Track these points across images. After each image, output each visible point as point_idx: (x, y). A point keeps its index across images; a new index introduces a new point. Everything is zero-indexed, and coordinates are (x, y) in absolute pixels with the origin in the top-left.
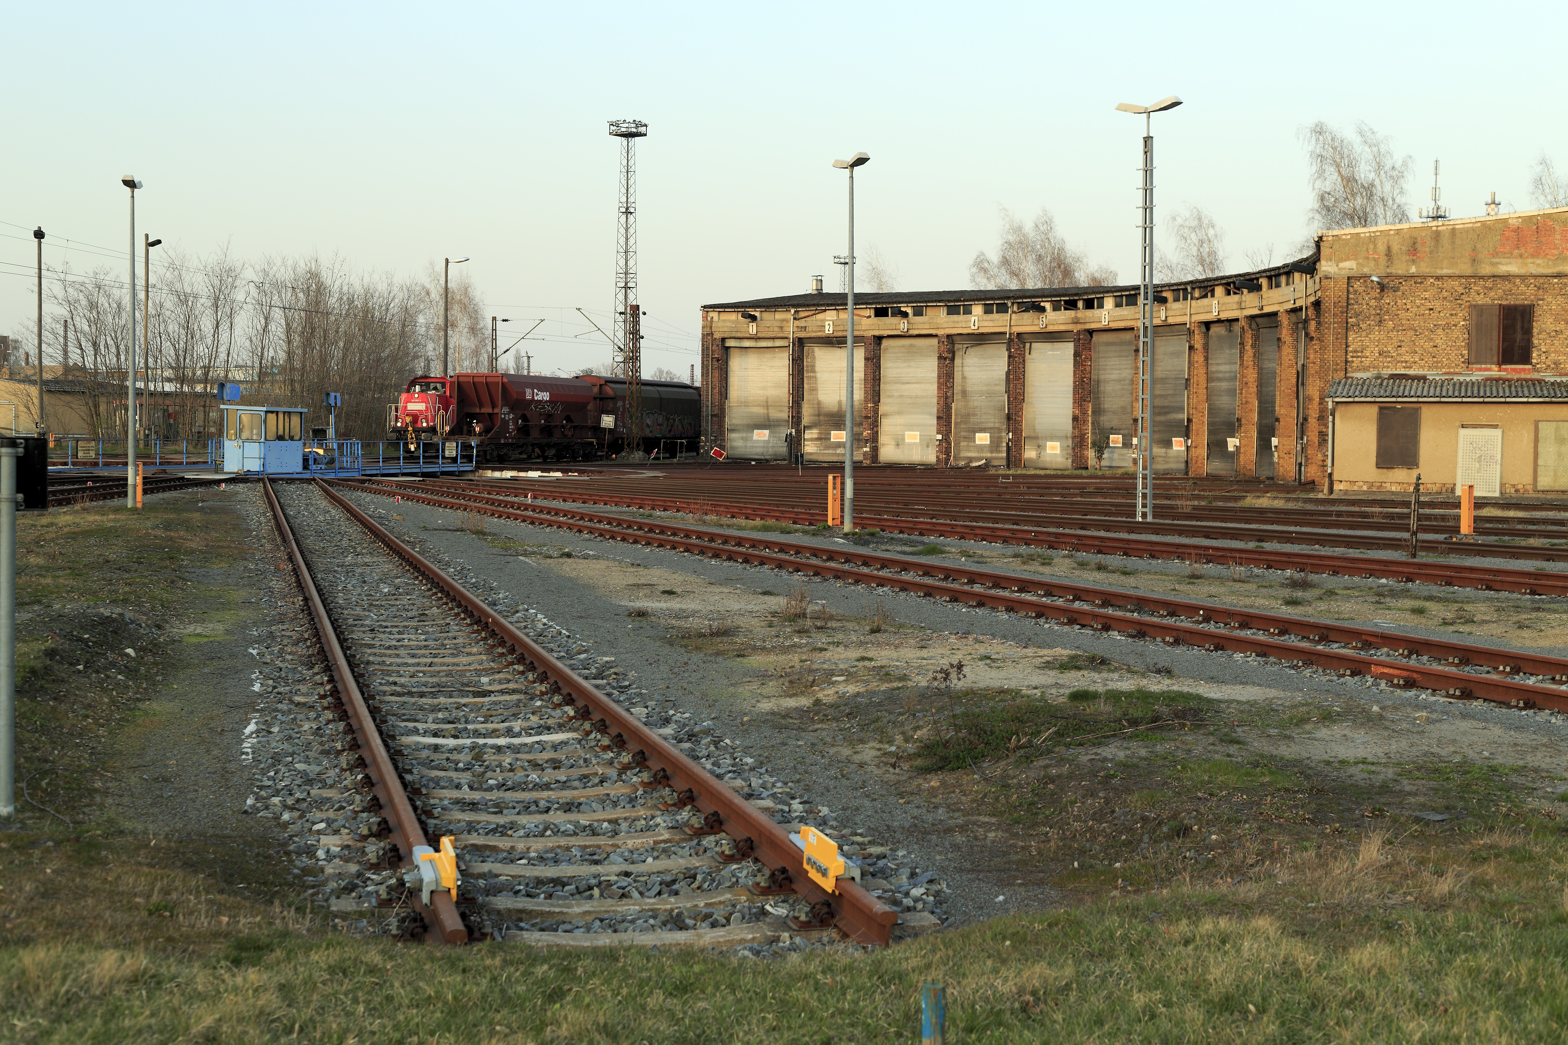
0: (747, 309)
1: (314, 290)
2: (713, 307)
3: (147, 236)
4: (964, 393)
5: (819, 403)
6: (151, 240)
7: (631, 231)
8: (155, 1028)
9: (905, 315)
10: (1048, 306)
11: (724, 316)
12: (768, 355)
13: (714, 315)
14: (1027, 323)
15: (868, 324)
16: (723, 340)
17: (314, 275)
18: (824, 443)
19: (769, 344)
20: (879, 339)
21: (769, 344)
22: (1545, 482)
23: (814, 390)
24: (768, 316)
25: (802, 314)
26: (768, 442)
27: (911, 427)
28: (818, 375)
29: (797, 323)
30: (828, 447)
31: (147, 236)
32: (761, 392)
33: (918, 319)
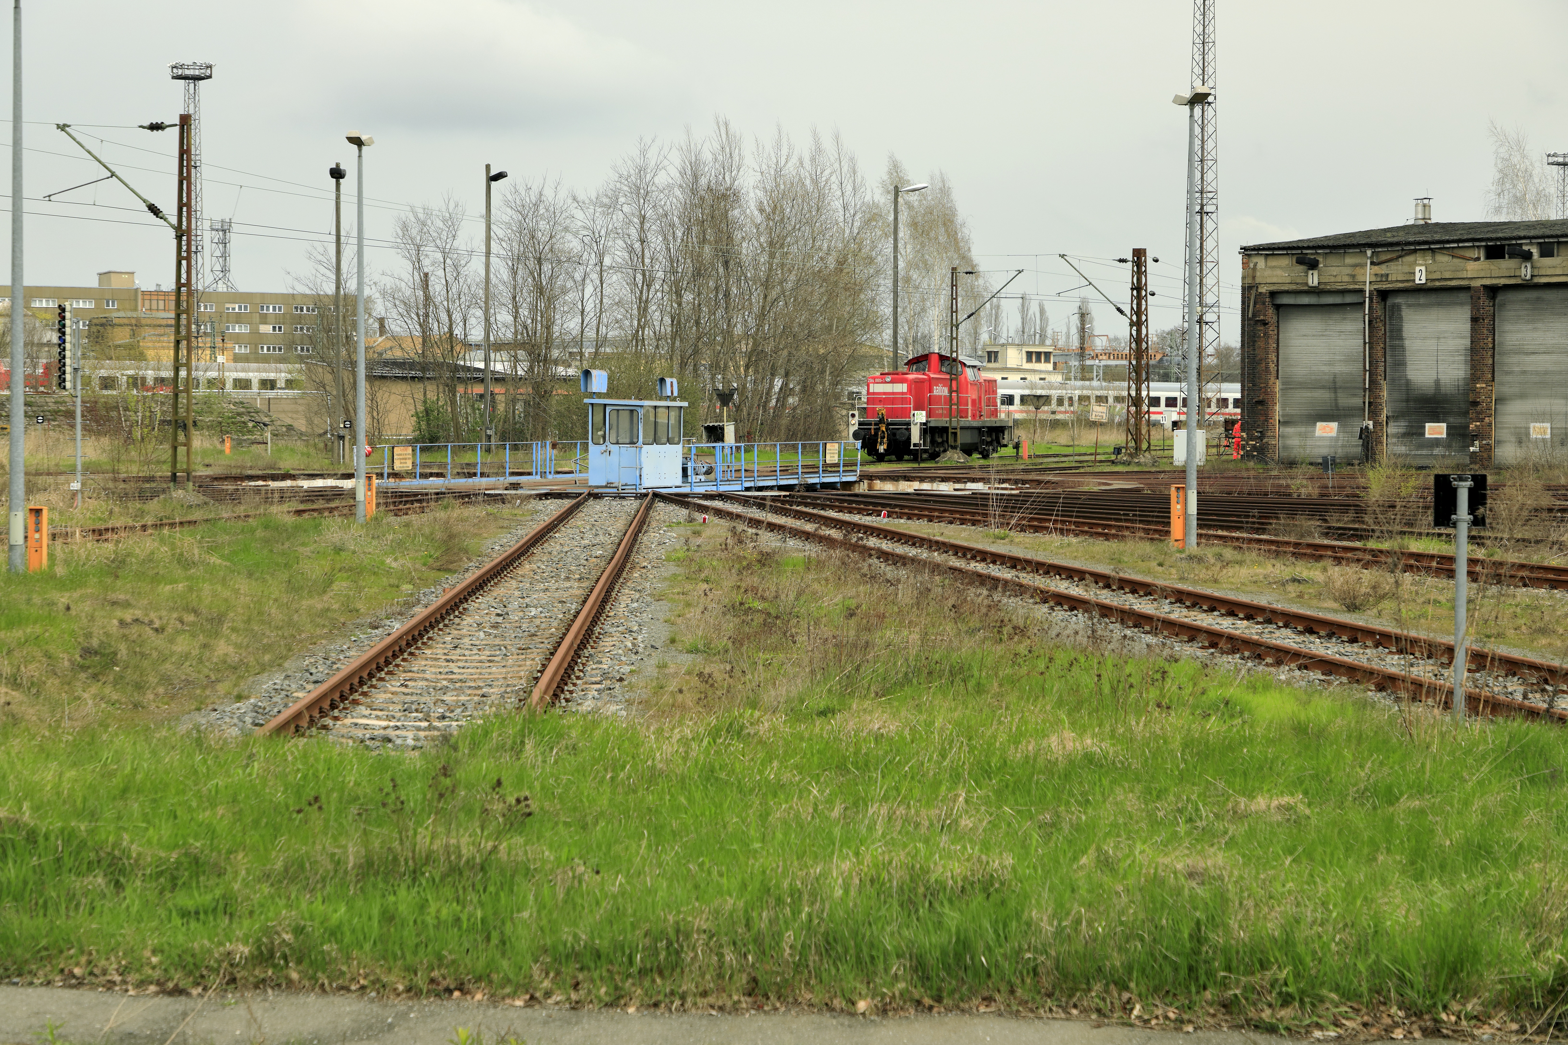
0: (1305, 253)
1: (710, 209)
2: (1257, 249)
3: (488, 167)
4: (1330, 363)
5: (1408, 382)
6: (493, 172)
7: (1210, 129)
8: (452, 987)
9: (1527, 256)
10: (1535, 251)
11: (1273, 262)
12: (1336, 316)
13: (1261, 262)
14: (1501, 271)
15: (1478, 270)
16: (1273, 294)
17: (710, 209)
18: (1415, 440)
19: (1338, 300)
20: (1493, 291)
21: (1338, 300)
22: (25, 216)
23: (1400, 364)
24: (1333, 260)
25: (1383, 257)
26: (1337, 439)
27: (1540, 417)
28: (1407, 343)
30: (1421, 446)
31: (488, 167)
32: (1326, 369)
33: (1547, 261)
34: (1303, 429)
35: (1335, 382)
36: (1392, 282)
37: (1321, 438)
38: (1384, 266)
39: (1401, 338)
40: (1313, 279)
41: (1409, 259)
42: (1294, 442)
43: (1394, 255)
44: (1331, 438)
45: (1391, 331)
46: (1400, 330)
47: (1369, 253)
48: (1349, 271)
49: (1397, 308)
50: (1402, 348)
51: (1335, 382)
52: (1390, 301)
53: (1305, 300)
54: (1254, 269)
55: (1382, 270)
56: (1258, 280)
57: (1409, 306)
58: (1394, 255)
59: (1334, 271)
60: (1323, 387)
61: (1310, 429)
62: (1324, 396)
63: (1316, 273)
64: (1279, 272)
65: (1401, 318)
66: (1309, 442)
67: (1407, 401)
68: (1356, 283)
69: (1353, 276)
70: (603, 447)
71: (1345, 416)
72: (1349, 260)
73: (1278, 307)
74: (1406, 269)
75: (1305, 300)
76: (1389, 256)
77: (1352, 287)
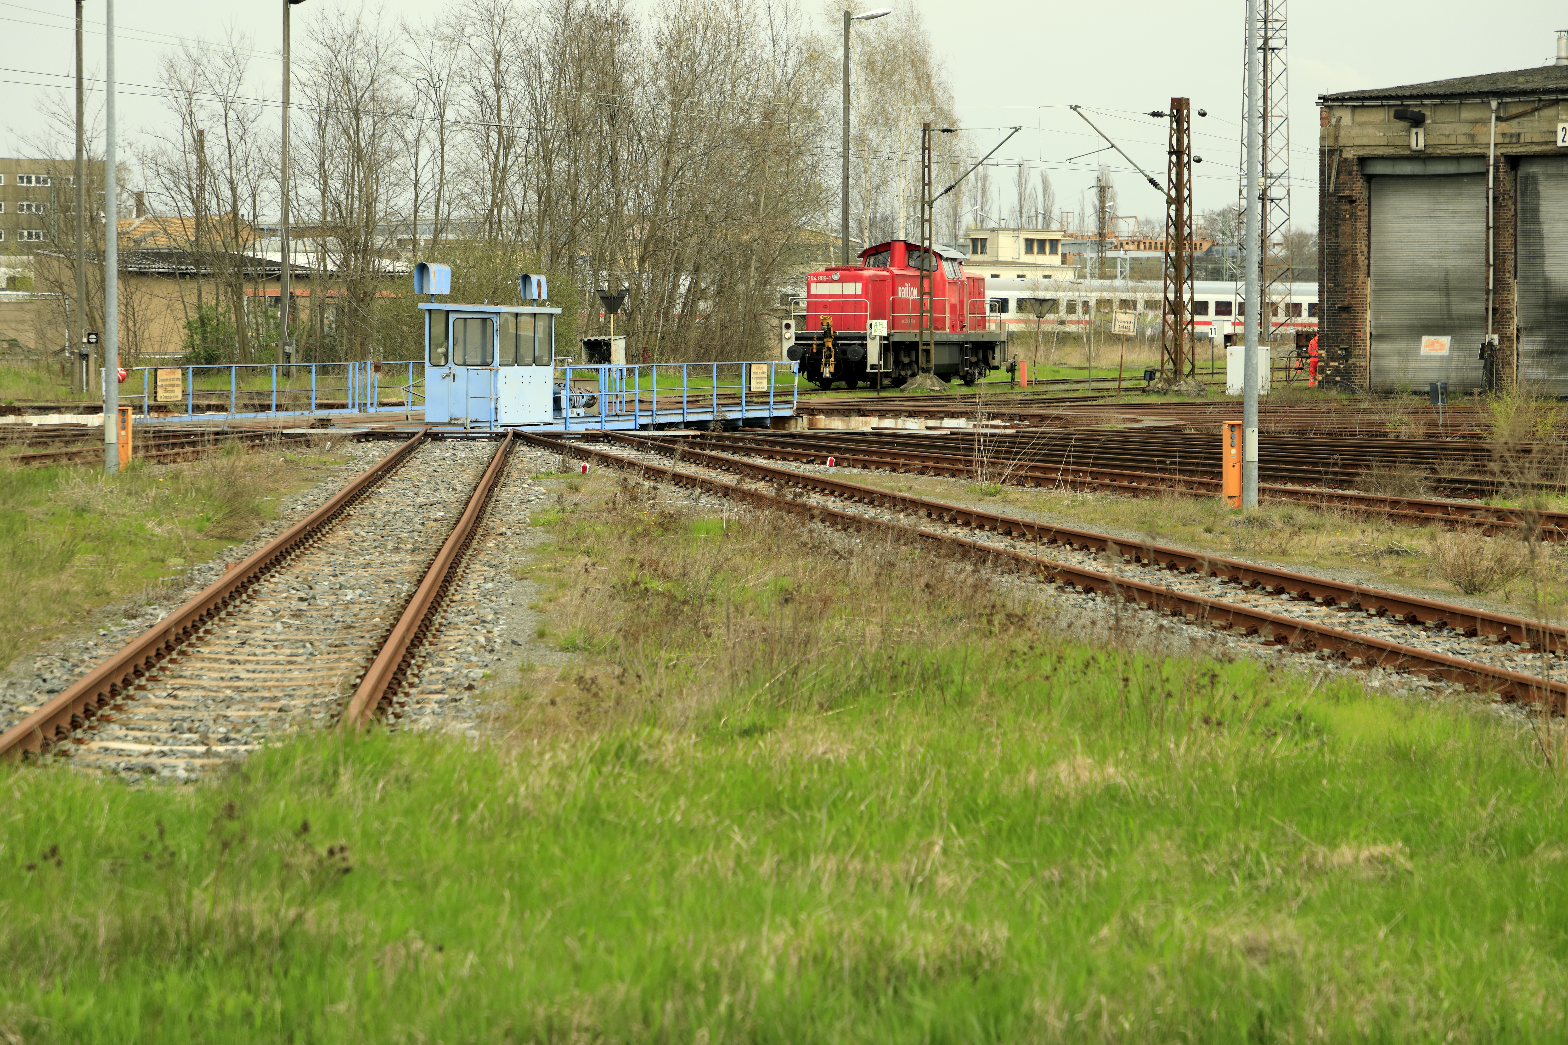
4: (1441, 255)
5: (1547, 282)
11: (1363, 116)
12: (1449, 191)
13: (1346, 117)
16: (1363, 161)
21: (1451, 168)
23: (1536, 256)
25: (1514, 110)
26: (1449, 359)
28: (1546, 228)
29: (1504, 126)
32: (1434, 263)
34: (1403, 346)
35: (1446, 281)
36: (1525, 144)
37: (1429, 358)
38: (1514, 123)
39: (1537, 221)
40: (1418, 140)
41: (1549, 112)
42: (1392, 363)
43: (1528, 108)
44: (1442, 357)
45: (1524, 211)
46: (1536, 210)
47: (1494, 104)
48: (1465, 128)
49: (1531, 181)
50: (1539, 234)
51: (1446, 281)
52: (1522, 171)
53: (1407, 169)
54: (1337, 126)
55: (1512, 127)
56: (1342, 142)
57: (1549, 177)
58: (1528, 108)
59: (1447, 129)
60: (1431, 288)
61: (1413, 345)
62: (1432, 299)
63: (1421, 132)
64: (1371, 130)
65: (1537, 194)
66: (1412, 364)
67: (1546, 306)
68: (1475, 145)
69: (1473, 136)
70: (445, 370)
71: (1461, 327)
72: (1467, 114)
73: (1369, 179)
74: (1545, 127)
75: (1407, 169)
76: (1521, 109)
77: (1470, 151)
